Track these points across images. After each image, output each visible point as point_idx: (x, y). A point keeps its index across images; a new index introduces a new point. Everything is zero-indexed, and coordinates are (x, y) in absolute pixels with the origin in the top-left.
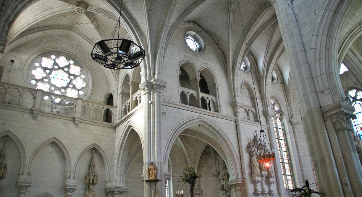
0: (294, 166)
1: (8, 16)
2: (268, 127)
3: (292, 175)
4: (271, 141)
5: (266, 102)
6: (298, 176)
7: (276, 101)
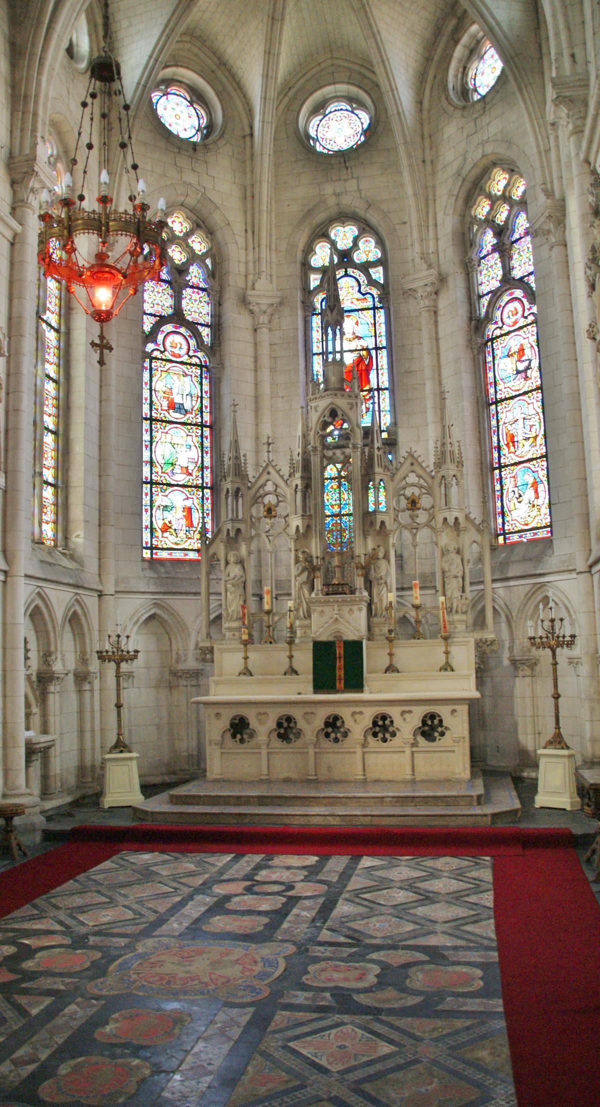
0: (79, 449)
1: (6, 1003)
2: (15, 236)
3: (62, 486)
4: (15, 302)
5: (35, 114)
6: (85, 493)
7: (61, 153)
